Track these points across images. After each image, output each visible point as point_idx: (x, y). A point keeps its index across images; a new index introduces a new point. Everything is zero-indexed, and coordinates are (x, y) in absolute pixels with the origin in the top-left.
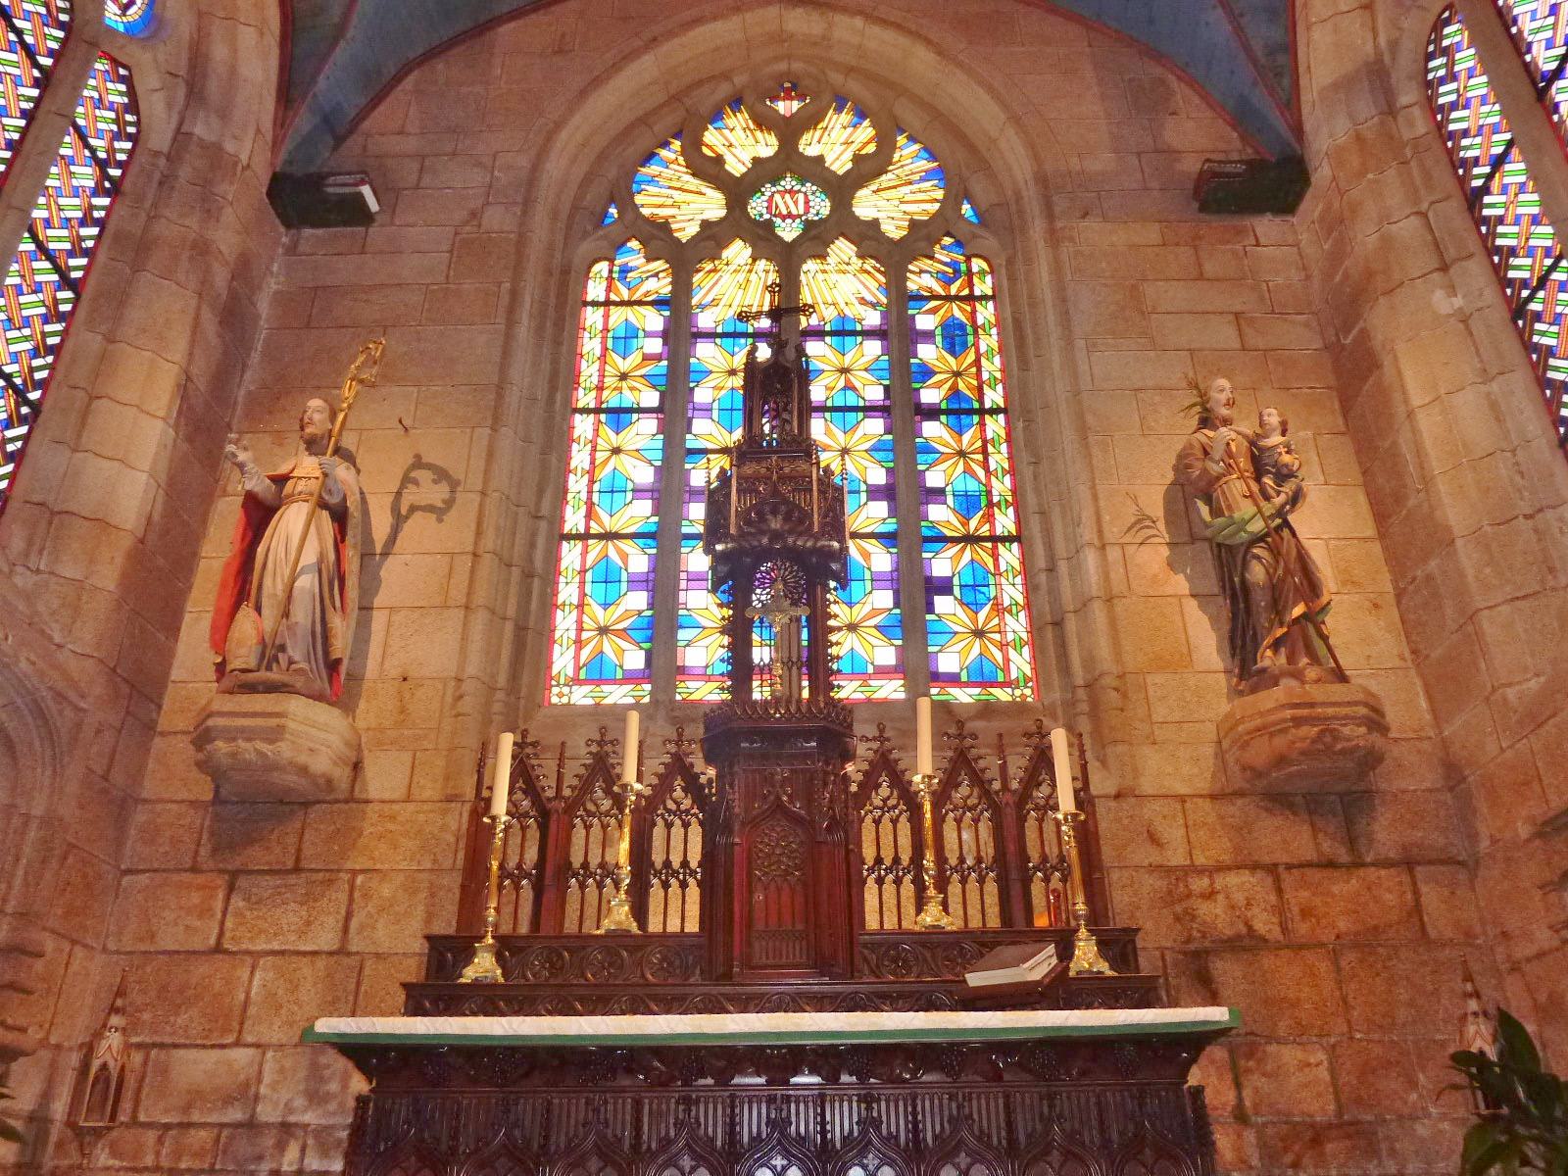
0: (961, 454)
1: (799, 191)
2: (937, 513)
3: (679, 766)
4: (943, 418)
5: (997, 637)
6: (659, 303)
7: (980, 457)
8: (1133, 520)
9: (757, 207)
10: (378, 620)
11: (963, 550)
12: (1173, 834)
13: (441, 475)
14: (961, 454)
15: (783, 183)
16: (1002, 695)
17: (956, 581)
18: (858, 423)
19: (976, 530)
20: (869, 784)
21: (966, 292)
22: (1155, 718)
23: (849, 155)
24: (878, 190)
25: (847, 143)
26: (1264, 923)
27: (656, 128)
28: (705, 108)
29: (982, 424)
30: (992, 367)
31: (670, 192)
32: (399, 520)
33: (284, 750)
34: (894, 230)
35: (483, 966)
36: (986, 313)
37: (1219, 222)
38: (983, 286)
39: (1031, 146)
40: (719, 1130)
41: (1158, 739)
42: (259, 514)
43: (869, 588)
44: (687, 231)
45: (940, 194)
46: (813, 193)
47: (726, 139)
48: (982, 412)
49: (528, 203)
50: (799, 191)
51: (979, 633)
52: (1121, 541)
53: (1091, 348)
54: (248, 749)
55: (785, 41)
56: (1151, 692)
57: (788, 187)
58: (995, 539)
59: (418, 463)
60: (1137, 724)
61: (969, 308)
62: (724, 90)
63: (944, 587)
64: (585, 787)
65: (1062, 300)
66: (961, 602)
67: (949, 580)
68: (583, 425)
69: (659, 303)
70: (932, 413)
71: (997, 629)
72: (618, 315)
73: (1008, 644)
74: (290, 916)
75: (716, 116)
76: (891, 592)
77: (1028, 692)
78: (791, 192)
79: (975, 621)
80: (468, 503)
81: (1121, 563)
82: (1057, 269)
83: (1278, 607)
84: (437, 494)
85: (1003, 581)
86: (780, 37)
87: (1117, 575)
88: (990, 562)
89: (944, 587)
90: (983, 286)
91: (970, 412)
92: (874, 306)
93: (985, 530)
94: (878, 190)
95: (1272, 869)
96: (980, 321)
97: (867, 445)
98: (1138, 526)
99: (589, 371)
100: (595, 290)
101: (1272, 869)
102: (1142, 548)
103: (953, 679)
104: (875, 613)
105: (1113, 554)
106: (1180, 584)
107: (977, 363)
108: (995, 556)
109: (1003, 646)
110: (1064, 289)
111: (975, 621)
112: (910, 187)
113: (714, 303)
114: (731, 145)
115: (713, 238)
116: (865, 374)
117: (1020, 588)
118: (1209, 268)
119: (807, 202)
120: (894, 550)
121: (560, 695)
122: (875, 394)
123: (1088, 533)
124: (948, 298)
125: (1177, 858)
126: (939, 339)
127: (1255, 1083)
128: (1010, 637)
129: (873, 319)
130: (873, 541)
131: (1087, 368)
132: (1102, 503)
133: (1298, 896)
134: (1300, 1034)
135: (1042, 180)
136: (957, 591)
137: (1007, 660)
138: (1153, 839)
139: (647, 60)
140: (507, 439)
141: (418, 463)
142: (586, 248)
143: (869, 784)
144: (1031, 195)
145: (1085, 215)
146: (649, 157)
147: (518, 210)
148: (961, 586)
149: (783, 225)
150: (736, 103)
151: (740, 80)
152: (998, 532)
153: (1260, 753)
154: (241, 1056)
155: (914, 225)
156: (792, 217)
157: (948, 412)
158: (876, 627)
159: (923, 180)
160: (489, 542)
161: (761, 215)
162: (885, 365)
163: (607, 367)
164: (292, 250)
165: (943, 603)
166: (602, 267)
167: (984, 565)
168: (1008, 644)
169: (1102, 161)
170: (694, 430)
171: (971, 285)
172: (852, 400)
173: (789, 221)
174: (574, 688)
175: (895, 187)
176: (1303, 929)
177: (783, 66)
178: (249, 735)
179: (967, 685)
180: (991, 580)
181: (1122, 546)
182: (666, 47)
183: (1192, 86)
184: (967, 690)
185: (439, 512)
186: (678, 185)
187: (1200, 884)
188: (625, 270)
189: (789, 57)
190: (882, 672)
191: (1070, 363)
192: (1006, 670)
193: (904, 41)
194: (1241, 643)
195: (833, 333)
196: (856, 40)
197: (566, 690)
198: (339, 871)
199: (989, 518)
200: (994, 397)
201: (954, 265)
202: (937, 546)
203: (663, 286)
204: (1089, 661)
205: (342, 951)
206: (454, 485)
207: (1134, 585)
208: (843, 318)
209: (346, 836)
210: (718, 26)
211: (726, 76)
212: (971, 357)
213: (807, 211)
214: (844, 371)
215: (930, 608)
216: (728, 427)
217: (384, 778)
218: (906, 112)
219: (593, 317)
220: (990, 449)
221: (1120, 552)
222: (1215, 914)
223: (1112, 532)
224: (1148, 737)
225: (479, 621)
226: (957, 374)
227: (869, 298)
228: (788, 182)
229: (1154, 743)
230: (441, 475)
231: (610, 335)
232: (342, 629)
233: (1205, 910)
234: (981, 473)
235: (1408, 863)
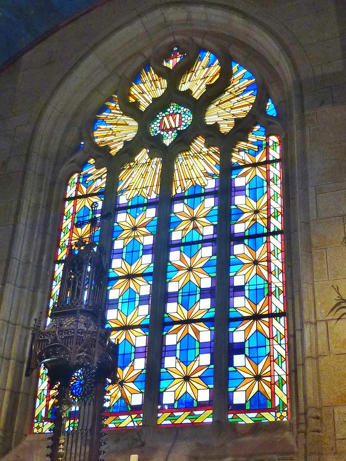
0: (256, 262)
1: (177, 113)
2: (239, 302)
4: (246, 241)
5: (269, 379)
7: (266, 264)
8: (335, 303)
9: (155, 128)
11: (252, 325)
14: (256, 262)
15: (169, 110)
16: (269, 417)
17: (247, 345)
18: (198, 251)
19: (260, 310)
21: (264, 159)
22: (338, 436)
23: (204, 86)
24: (220, 104)
25: (205, 78)
27: (104, 92)
28: (129, 73)
29: (268, 242)
31: (111, 126)
34: (225, 128)
41: (339, 450)
43: (197, 353)
46: (185, 113)
47: (141, 89)
48: (269, 234)
50: (177, 113)
51: (258, 378)
52: (326, 318)
53: (319, 191)
55: (169, 26)
56: (337, 419)
57: (171, 112)
58: (271, 315)
60: (326, 440)
61: (265, 169)
62: (140, 60)
63: (240, 349)
66: (248, 357)
67: (242, 344)
70: (240, 239)
71: (269, 374)
72: (80, 203)
73: (275, 383)
75: (136, 78)
76: (209, 354)
77: (284, 414)
78: (173, 114)
79: (256, 370)
81: (326, 332)
85: (275, 343)
86: (166, 24)
87: (322, 340)
88: (267, 330)
89: (240, 349)
91: (262, 235)
92: (212, 176)
93: (265, 311)
94: (220, 104)
96: (271, 176)
97: (201, 265)
98: (338, 307)
100: (71, 192)
102: (339, 321)
103: (241, 408)
104: (200, 368)
107: (268, 204)
108: (270, 326)
109: (272, 385)
110: (12, 305)
111: (256, 370)
112: (238, 98)
113: (128, 189)
114: (143, 93)
116: (204, 220)
117: (284, 346)
119: (180, 119)
120: (213, 328)
121: (38, 427)
122: (209, 231)
124: (254, 165)
126: (247, 192)
128: (276, 378)
129: (211, 184)
130: (202, 324)
131: (314, 205)
132: (317, 294)
136: (247, 351)
137: (273, 393)
139: (92, 58)
145: (322, 104)
146: (104, 108)
147: (23, 158)
148: (249, 348)
149: (167, 135)
150: (146, 66)
151: (148, 53)
152: (273, 311)
155: (238, 121)
156: (172, 129)
157: (249, 237)
158: (199, 377)
159: (245, 91)
161: (156, 132)
162: (216, 212)
163: (74, 235)
165: (239, 360)
167: (263, 334)
168: (275, 383)
170: (113, 266)
171: (267, 154)
172: (196, 237)
173: (170, 132)
174: (45, 423)
175: (229, 100)
177: (170, 39)
179: (250, 411)
180: (268, 342)
181: (327, 321)
182: (101, 47)
183: (78, 179)
184: (249, 415)
186: (114, 121)
188: (86, 176)
189: (173, 34)
190: (202, 406)
192: (273, 400)
193: (226, 14)
195: (188, 197)
196: (203, 18)
197: (41, 425)
200: (277, 224)
202: (238, 323)
203: (101, 183)
207: (332, 348)
208: (195, 186)
210: (128, 29)
211: (140, 53)
212: (265, 199)
213: (179, 126)
214: (193, 219)
215: (231, 363)
216: (130, 263)
218: (234, 51)
219: (69, 207)
220: (272, 257)
221: (325, 325)
224: (332, 449)
226: (256, 212)
227: (210, 171)
228: (172, 108)
229: (335, 453)
231: (76, 216)
234: (265, 273)
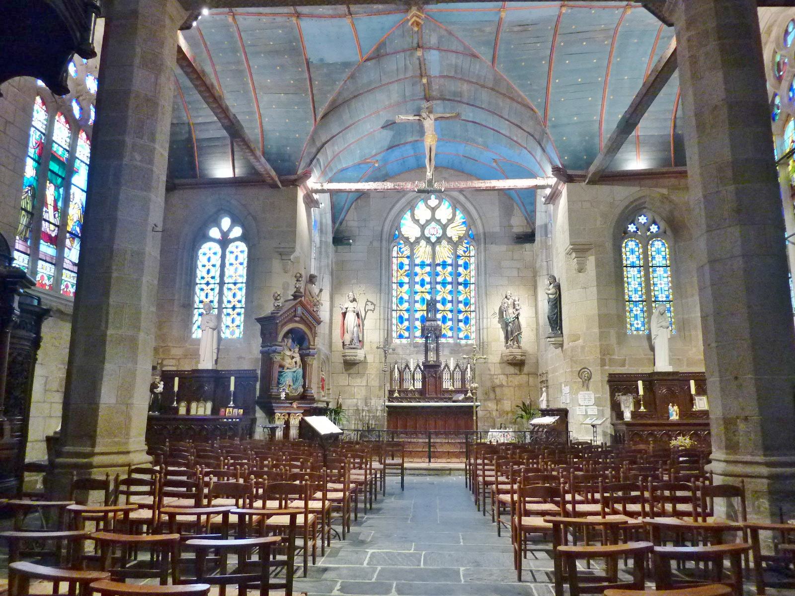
3: (418, 365)
6: (408, 257)
10: (365, 331)
12: (492, 369)
13: (372, 303)
20: (444, 368)
26: (504, 383)
30: (473, 273)
32: (366, 313)
33: (357, 358)
35: (396, 395)
36: (472, 260)
37: (518, 247)
38: (472, 253)
39: (483, 225)
40: (93, 19)
42: (344, 314)
44: (412, 240)
45: (465, 229)
49: (381, 240)
53: (490, 276)
54: (352, 358)
59: (368, 301)
64: (405, 368)
65: (485, 264)
68: (394, 286)
69: (408, 257)
74: (359, 380)
80: (377, 309)
82: (485, 257)
83: (512, 334)
84: (372, 307)
87: (489, 324)
90: (472, 253)
95: (507, 375)
99: (395, 274)
100: (395, 254)
101: (507, 375)
105: (489, 320)
106: (499, 326)
115: (417, 241)
118: (515, 257)
123: (485, 316)
125: (492, 373)
127: (499, 406)
133: (510, 379)
134: (507, 399)
135: (485, 234)
138: (489, 370)
140: (383, 294)
141: (368, 301)
142: (393, 244)
143: (444, 368)
144: (482, 236)
153: (505, 359)
154: (355, 400)
160: (382, 317)
164: (336, 251)
166: (396, 248)
169: (497, 229)
176: (510, 384)
178: (352, 356)
185: (373, 311)
187: (495, 377)
191: (485, 280)
194: (507, 338)
198: (92, 454)
199: (470, 307)
201: (467, 248)
204: (483, 339)
205: (367, 386)
206: (375, 305)
209: (365, 368)
217: (370, 359)
219: (394, 260)
222: (497, 382)
223: (489, 315)
225: (382, 332)
230: (372, 303)
232: (361, 335)
233: (495, 381)
235: (528, 374)
